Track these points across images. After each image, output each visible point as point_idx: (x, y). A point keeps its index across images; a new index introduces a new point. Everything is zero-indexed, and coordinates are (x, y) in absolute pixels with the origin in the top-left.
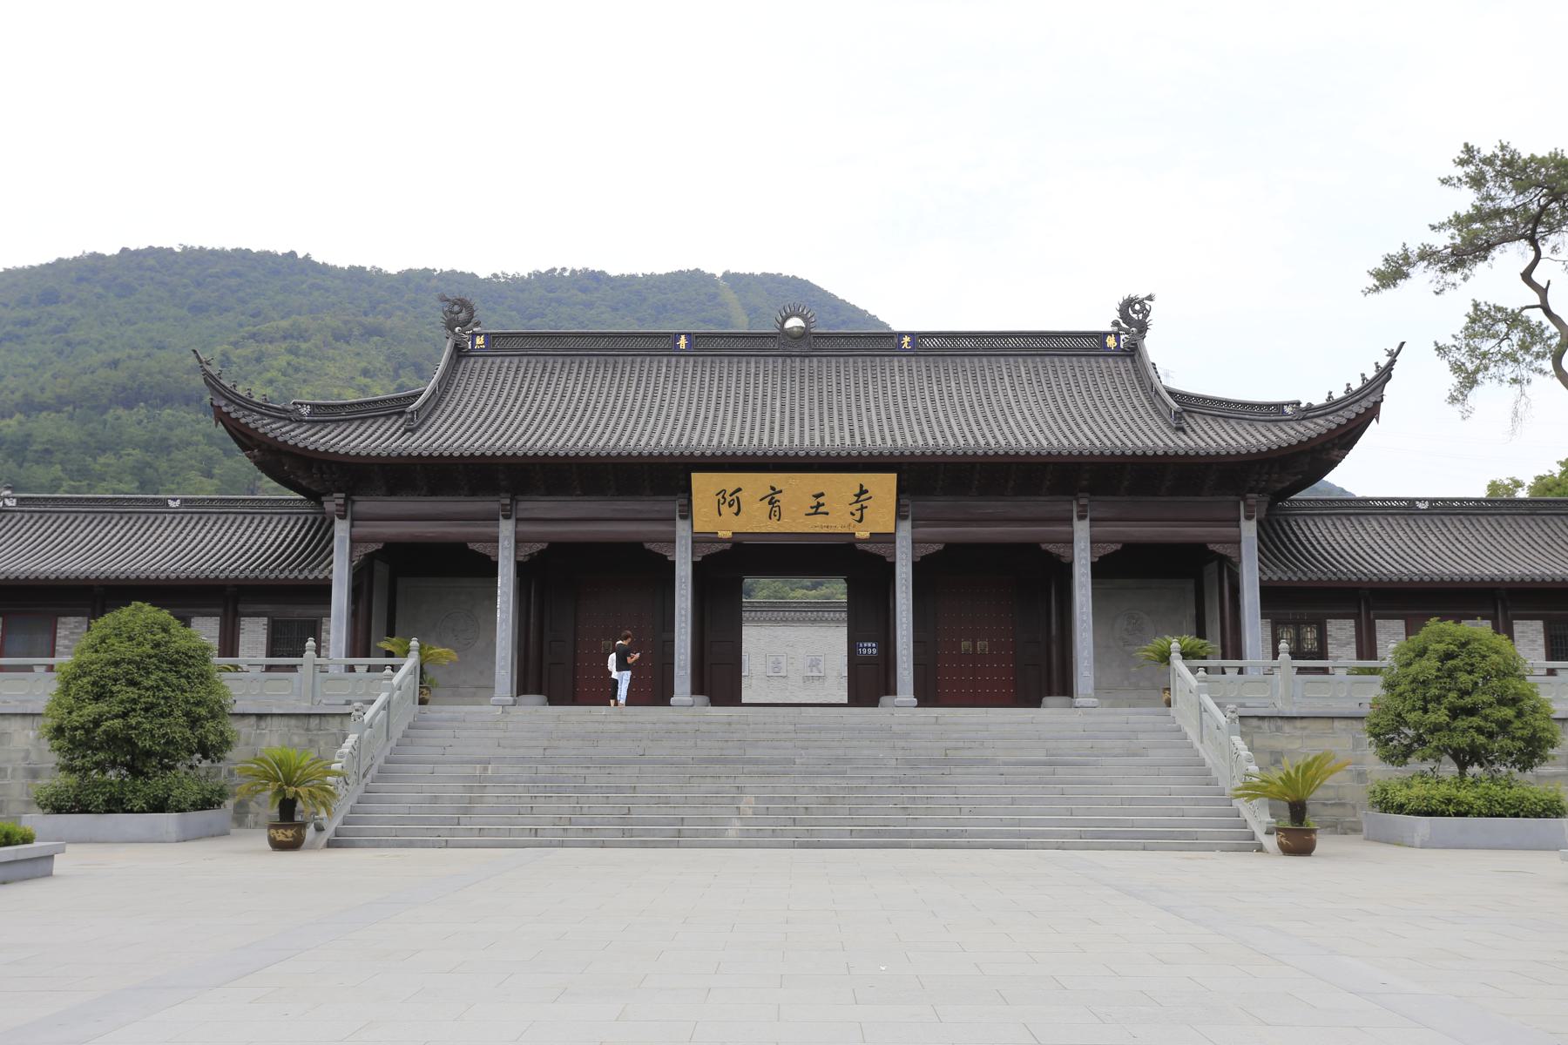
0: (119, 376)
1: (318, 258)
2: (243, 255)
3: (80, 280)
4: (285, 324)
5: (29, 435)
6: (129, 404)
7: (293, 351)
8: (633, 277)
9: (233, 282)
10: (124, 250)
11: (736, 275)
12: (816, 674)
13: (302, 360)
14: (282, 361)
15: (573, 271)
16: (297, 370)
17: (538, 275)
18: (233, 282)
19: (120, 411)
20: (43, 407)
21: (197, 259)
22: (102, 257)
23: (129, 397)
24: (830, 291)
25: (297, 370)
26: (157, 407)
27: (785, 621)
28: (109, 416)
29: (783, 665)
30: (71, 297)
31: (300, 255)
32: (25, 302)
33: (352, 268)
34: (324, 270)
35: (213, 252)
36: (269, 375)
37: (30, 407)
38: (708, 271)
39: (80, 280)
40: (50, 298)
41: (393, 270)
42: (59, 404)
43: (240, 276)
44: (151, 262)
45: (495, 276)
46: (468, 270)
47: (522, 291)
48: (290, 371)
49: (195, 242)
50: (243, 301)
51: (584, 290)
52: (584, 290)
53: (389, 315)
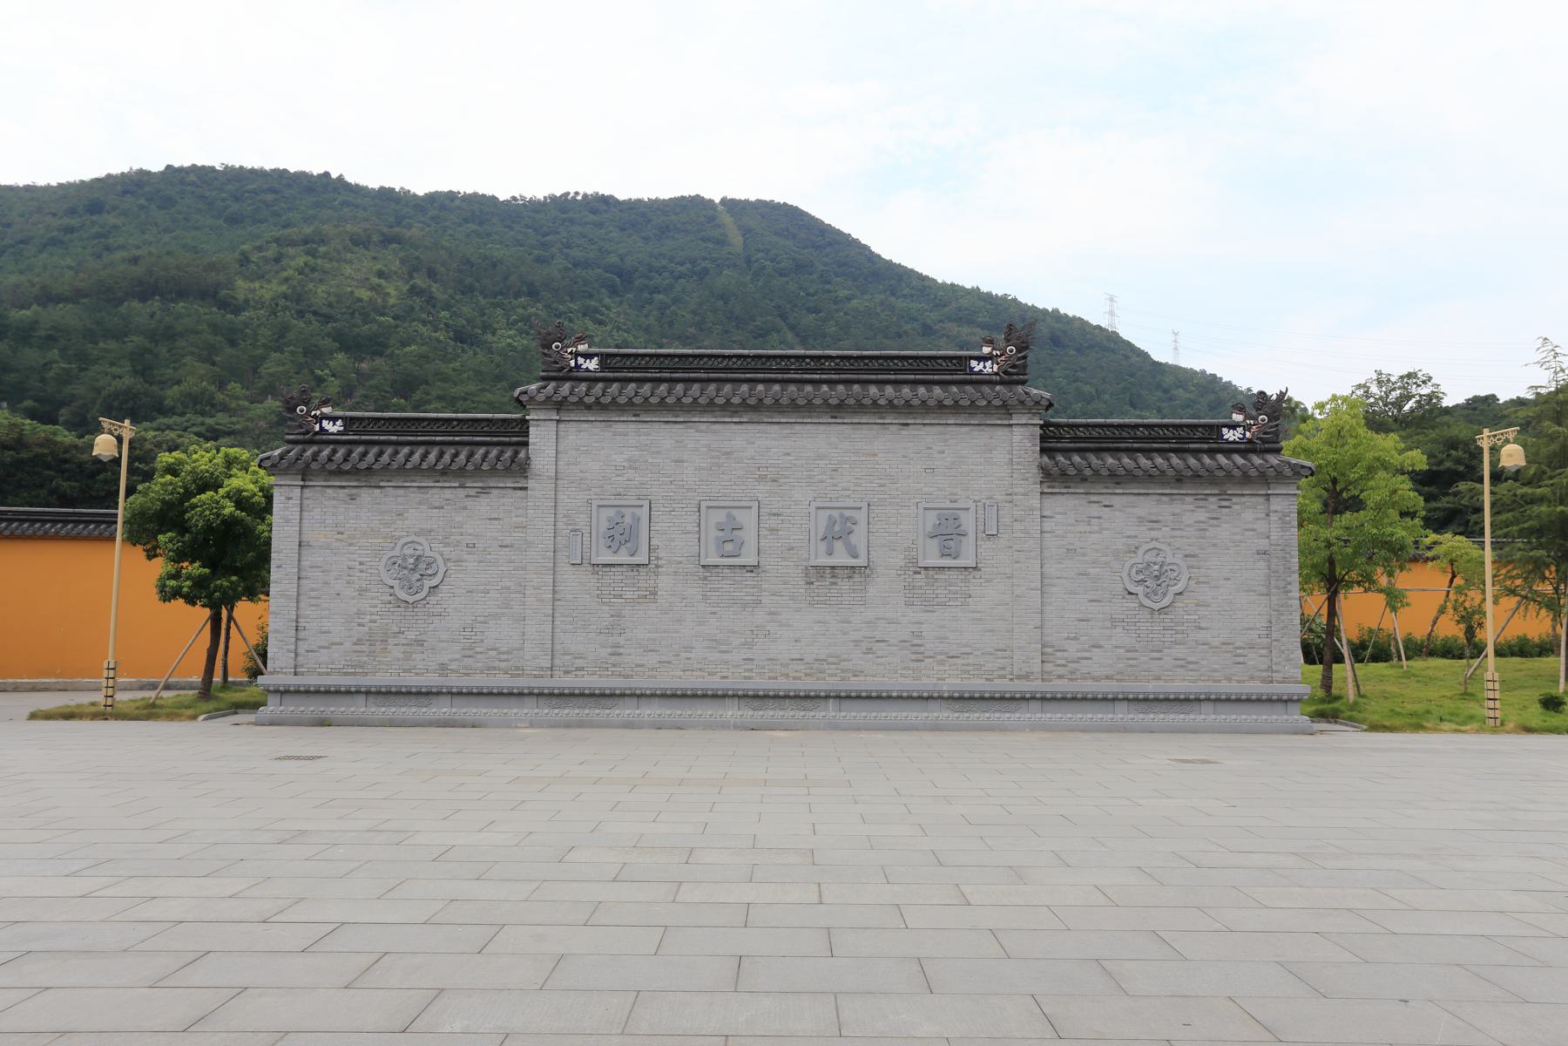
0: (138, 270)
1: (351, 179)
2: (281, 174)
3: (125, 192)
4: (308, 230)
5: (36, 322)
6: (143, 298)
7: (312, 253)
8: (639, 201)
9: (269, 197)
10: (169, 167)
11: (733, 201)
12: (841, 558)
13: (319, 261)
14: (301, 261)
15: (585, 196)
16: (313, 270)
17: (553, 198)
18: (269, 197)
19: (135, 304)
20: (60, 299)
21: (238, 179)
22: (148, 173)
23: (145, 290)
24: (817, 216)
25: (313, 270)
26: (172, 300)
27: (754, 409)
28: (123, 309)
29: (749, 535)
30: (114, 208)
31: (334, 176)
32: (72, 212)
33: (382, 189)
34: (357, 190)
35: (252, 171)
36: (285, 274)
37: (47, 298)
38: (707, 196)
39: (125, 192)
40: (95, 208)
41: (421, 193)
42: (76, 296)
43: (275, 192)
44: (192, 178)
45: (514, 198)
46: (489, 193)
47: (538, 212)
48: (307, 270)
49: (236, 162)
50: (276, 214)
51: (594, 212)
52: (594, 212)
53: (410, 227)
